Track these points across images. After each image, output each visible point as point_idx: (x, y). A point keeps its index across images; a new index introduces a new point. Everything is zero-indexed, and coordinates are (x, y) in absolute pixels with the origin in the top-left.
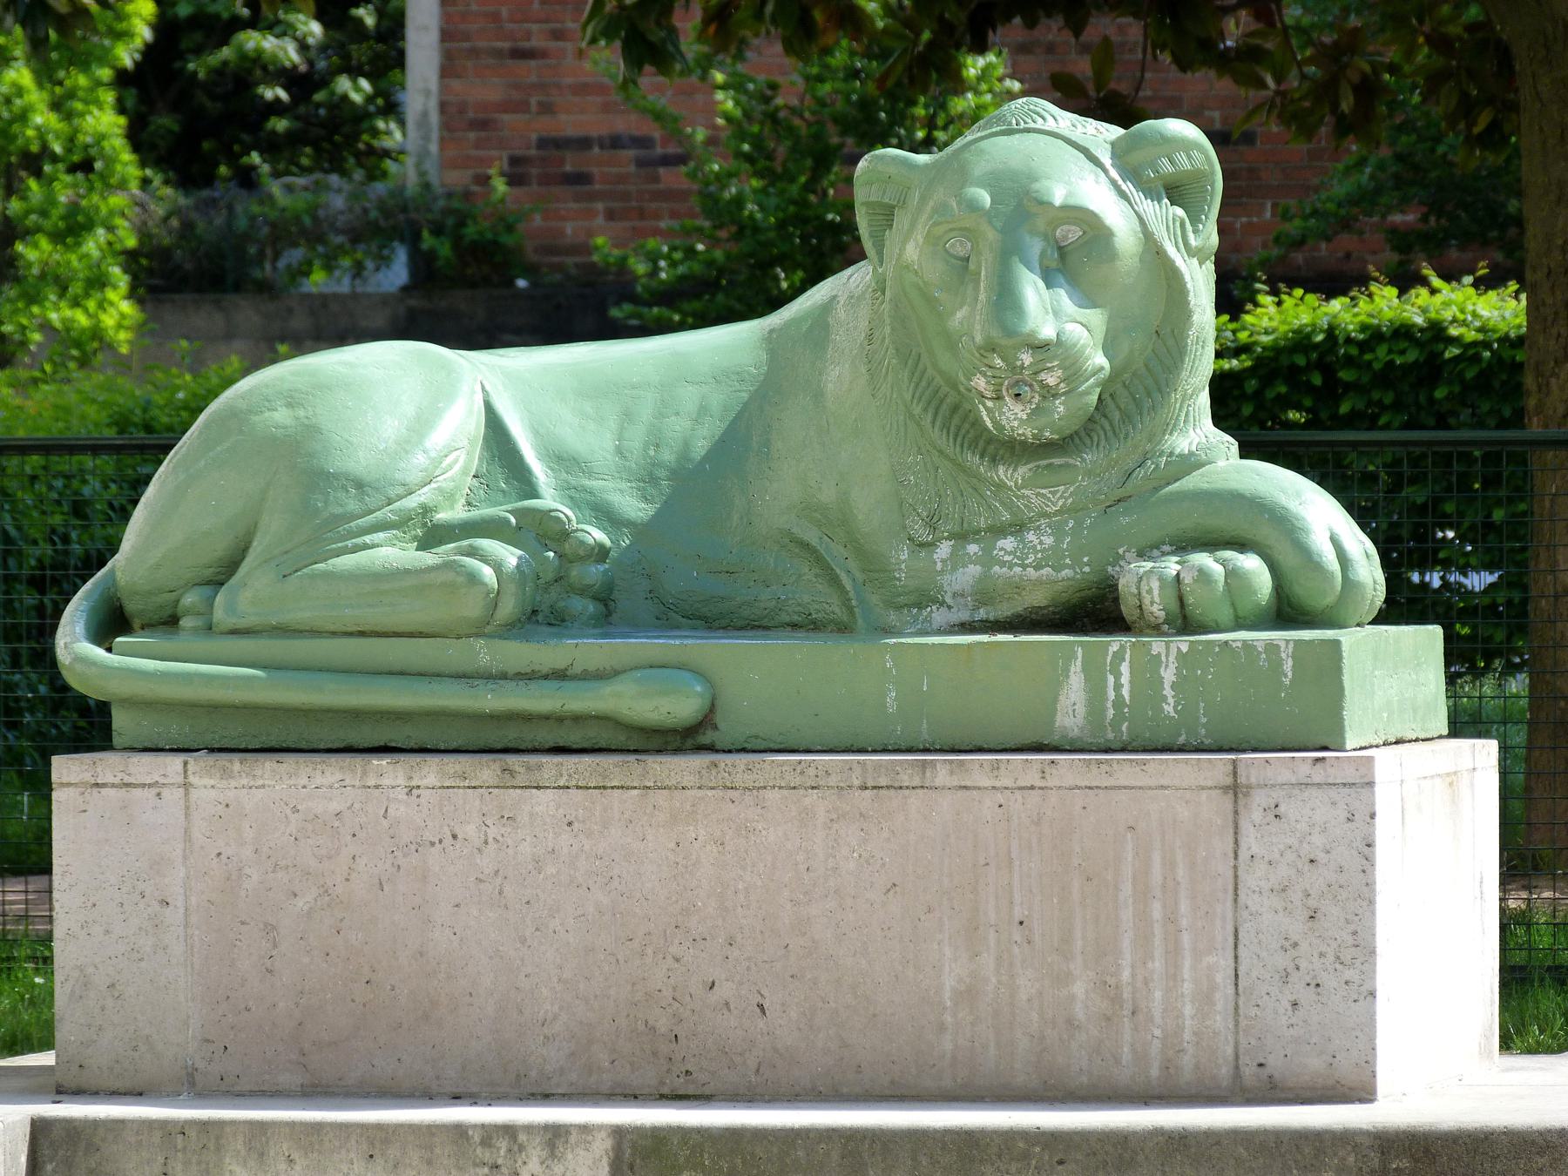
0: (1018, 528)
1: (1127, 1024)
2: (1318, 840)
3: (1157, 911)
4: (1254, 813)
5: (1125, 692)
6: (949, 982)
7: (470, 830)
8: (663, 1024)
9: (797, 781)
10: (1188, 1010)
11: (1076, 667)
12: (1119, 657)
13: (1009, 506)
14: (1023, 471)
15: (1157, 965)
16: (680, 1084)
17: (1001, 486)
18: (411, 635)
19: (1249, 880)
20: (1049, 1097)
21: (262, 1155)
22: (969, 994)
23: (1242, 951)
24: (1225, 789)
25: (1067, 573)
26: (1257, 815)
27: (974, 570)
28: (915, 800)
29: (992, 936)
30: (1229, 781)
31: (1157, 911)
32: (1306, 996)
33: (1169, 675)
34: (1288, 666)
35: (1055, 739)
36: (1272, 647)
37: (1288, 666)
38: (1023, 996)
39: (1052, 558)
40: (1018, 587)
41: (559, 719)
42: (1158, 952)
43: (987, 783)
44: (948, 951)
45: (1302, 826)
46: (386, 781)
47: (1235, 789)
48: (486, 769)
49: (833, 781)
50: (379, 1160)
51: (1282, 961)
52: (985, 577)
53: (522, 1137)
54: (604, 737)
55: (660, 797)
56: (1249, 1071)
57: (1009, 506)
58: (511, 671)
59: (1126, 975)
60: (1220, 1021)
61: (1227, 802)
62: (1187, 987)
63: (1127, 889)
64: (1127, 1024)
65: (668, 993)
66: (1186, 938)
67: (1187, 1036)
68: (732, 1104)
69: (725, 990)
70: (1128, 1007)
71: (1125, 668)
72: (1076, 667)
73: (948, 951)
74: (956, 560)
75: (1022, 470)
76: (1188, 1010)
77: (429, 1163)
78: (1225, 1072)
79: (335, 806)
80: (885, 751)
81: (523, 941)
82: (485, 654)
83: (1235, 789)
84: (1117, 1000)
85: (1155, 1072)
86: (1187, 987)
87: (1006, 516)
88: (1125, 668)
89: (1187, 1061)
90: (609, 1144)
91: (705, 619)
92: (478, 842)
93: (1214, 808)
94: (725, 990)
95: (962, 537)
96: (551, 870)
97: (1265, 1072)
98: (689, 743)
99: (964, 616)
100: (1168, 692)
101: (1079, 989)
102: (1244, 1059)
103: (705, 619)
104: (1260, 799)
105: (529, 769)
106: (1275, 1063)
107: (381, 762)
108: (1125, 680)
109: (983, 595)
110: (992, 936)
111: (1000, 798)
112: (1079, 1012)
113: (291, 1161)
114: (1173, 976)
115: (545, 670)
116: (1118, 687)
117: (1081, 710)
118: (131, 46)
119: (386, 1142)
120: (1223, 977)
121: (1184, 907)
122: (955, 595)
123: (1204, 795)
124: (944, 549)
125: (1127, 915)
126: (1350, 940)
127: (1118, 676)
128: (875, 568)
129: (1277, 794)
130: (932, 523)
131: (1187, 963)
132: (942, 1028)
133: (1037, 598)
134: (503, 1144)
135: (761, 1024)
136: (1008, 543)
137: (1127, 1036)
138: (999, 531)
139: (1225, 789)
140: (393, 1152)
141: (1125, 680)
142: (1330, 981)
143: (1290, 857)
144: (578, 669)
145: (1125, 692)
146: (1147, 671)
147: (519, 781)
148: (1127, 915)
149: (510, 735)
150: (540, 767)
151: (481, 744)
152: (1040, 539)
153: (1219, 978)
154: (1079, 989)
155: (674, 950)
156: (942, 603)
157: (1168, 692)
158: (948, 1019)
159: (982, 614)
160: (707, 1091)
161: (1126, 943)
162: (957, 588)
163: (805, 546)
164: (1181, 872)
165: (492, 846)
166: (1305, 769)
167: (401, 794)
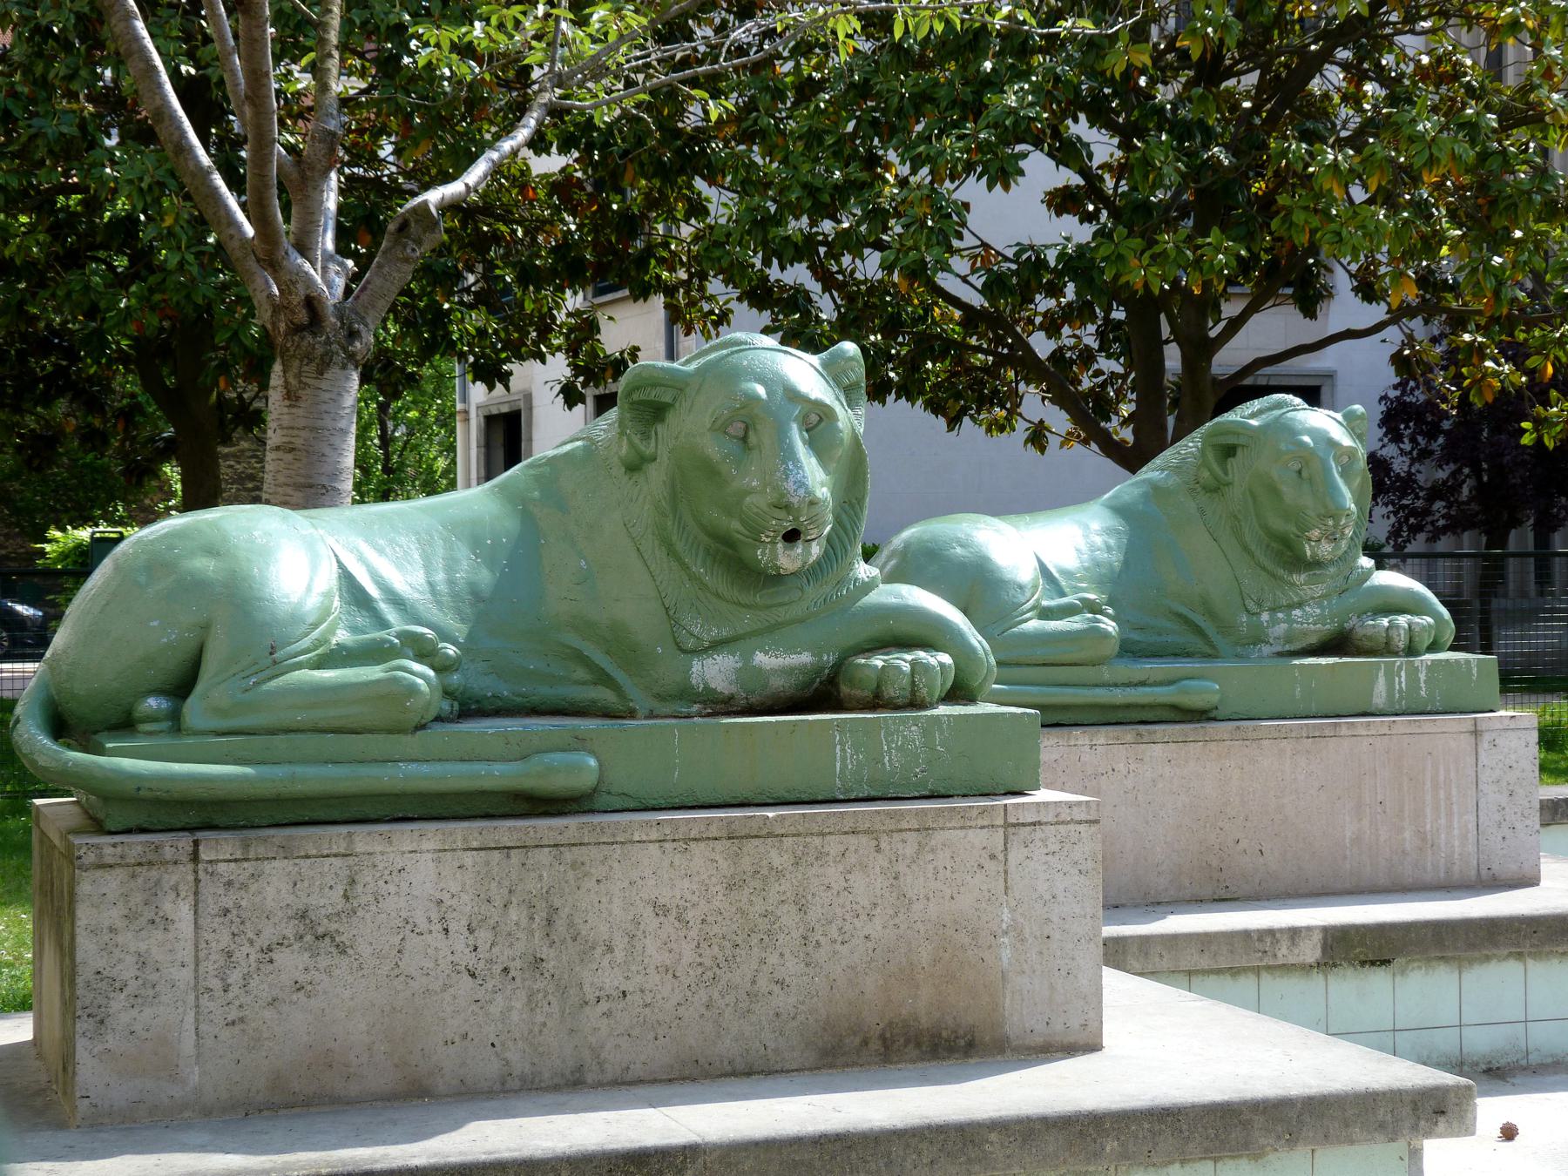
0: (1300, 605)
1: (1429, 852)
2: (1513, 757)
3: (1442, 795)
4: (1485, 744)
5: (1403, 685)
6: (1348, 834)
7: (1121, 767)
8: (1215, 863)
9: (1276, 735)
10: (1457, 843)
11: (1381, 673)
12: (1400, 668)
13: (1297, 594)
14: (1303, 577)
15: (1443, 821)
16: (1222, 893)
17: (1294, 584)
18: (1070, 665)
19: (1483, 778)
20: (39, 791)
21: (1146, 954)
22: (1357, 840)
23: (1480, 814)
24: (1471, 732)
25: (1328, 626)
26: (1486, 745)
27: (1284, 626)
28: (1332, 742)
29: (1368, 810)
30: (1473, 728)
31: (1442, 795)
32: (1508, 833)
33: (1422, 677)
34: (1475, 671)
35: (1373, 709)
36: (1468, 662)
37: (1475, 671)
38: (1382, 839)
39: (1321, 619)
40: (1305, 633)
41: (1128, 706)
42: (1443, 815)
43: (1365, 733)
44: (1347, 818)
45: (1506, 750)
46: (1080, 742)
47: (1476, 733)
48: (1128, 733)
49: (1293, 735)
50: (1206, 953)
51: (1497, 817)
52: (1290, 628)
53: (1278, 935)
54: (1166, 715)
55: (1212, 746)
56: (1484, 872)
57: (1297, 594)
58: (1119, 682)
59: (1428, 827)
60: (1471, 848)
61: (1473, 738)
62: (1456, 832)
63: (1428, 784)
64: (1429, 852)
65: (1217, 847)
66: (1455, 807)
67: (1456, 856)
68: (1281, 902)
69: (1243, 844)
70: (1430, 842)
71: (1403, 674)
72: (1381, 673)
73: (1347, 818)
74: (1274, 622)
75: (1303, 576)
76: (1457, 843)
77: (1232, 952)
78: (1473, 873)
79: (1054, 757)
80: (1295, 718)
81: (1147, 823)
82: (1106, 673)
83: (1476, 733)
84: (1424, 840)
85: (1442, 875)
86: (1456, 832)
87: (1296, 599)
88: (1403, 674)
89: (1456, 868)
90: (1321, 936)
91: (1132, 652)
92: (1125, 773)
93: (1466, 741)
94: (1243, 844)
95: (1273, 610)
96: (1161, 785)
97: (1491, 872)
98: (1204, 717)
99: (1279, 649)
100: (1422, 685)
101: (1407, 834)
102: (1482, 866)
103: (1132, 652)
104: (1487, 737)
105: (1150, 733)
106: (1496, 868)
107: (1077, 732)
108: (1403, 679)
109: (1288, 639)
110: (1368, 810)
111: (1371, 741)
112: (1408, 846)
113: (1161, 956)
114: (1450, 827)
115: (1135, 681)
116: (1400, 683)
117: (1384, 694)
118: (90, 418)
119: (1210, 942)
120: (1472, 826)
121: (1454, 792)
122: (1275, 638)
123: (1462, 736)
124: (1265, 616)
125: (1428, 797)
126: (1528, 805)
127: (1400, 677)
128: (1226, 628)
129: (1494, 735)
130: (1259, 604)
131: (1456, 820)
132: (1345, 858)
133: (1313, 640)
134: (1268, 940)
135: (1261, 860)
136: (1297, 612)
137: (1429, 858)
138: (1291, 607)
139: (1471, 732)
140: (1213, 948)
141: (1403, 679)
142: (1518, 826)
143: (1501, 765)
144: (1151, 680)
145: (1403, 685)
146: (1413, 672)
147: (1145, 740)
148: (1428, 797)
149: (1120, 716)
150: (1155, 732)
151: (1104, 721)
152: (1313, 610)
153: (1470, 826)
154: (1407, 834)
155: (1220, 824)
156: (1267, 643)
157: (1422, 685)
158: (1348, 853)
159: (1287, 647)
160: (1236, 896)
161: (1428, 811)
162: (1276, 635)
163: (1180, 615)
164: (1453, 775)
165: (1132, 774)
166: (1507, 722)
167: (1087, 748)
